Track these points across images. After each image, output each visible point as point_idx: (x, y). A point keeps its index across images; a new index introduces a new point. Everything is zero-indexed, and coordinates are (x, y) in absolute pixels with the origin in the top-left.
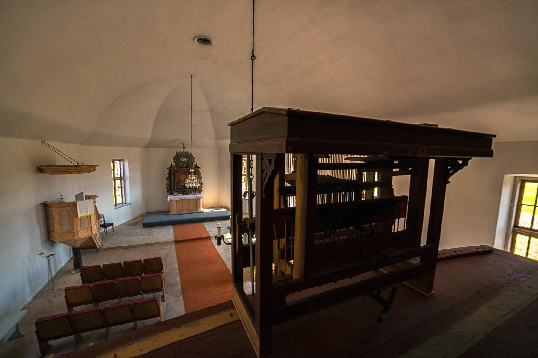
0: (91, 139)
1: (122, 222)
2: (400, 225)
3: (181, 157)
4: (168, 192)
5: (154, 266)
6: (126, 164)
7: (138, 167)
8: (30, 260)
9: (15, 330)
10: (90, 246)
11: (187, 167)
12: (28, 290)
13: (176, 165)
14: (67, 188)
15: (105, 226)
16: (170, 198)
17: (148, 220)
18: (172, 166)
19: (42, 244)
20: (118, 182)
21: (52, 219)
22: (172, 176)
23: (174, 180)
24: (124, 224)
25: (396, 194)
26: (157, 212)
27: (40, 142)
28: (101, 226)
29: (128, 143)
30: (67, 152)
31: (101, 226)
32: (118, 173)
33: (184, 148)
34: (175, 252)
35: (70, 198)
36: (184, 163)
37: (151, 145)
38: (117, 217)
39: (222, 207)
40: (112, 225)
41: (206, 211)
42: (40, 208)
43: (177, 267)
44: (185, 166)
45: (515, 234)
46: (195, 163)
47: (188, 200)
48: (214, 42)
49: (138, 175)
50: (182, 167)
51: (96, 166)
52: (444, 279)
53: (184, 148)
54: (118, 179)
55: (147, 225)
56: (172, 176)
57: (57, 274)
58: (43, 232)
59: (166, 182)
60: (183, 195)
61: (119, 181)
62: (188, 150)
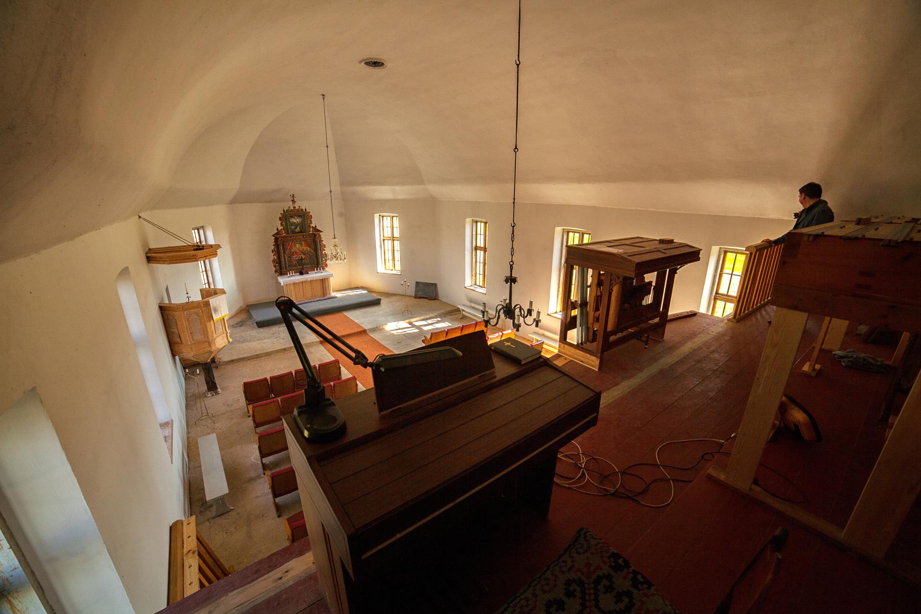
2: (649, 299)
3: (292, 217)
4: (276, 271)
11: (301, 232)
13: (286, 229)
16: (283, 280)
18: (279, 232)
22: (281, 248)
33: (293, 201)
35: (197, 297)
36: (296, 225)
39: (357, 288)
41: (339, 295)
44: (298, 230)
45: (715, 299)
46: (313, 225)
47: (312, 281)
48: (388, 64)
50: (293, 232)
52: (670, 331)
53: (293, 201)
56: (281, 248)
59: (272, 257)
60: (301, 274)
62: (301, 204)
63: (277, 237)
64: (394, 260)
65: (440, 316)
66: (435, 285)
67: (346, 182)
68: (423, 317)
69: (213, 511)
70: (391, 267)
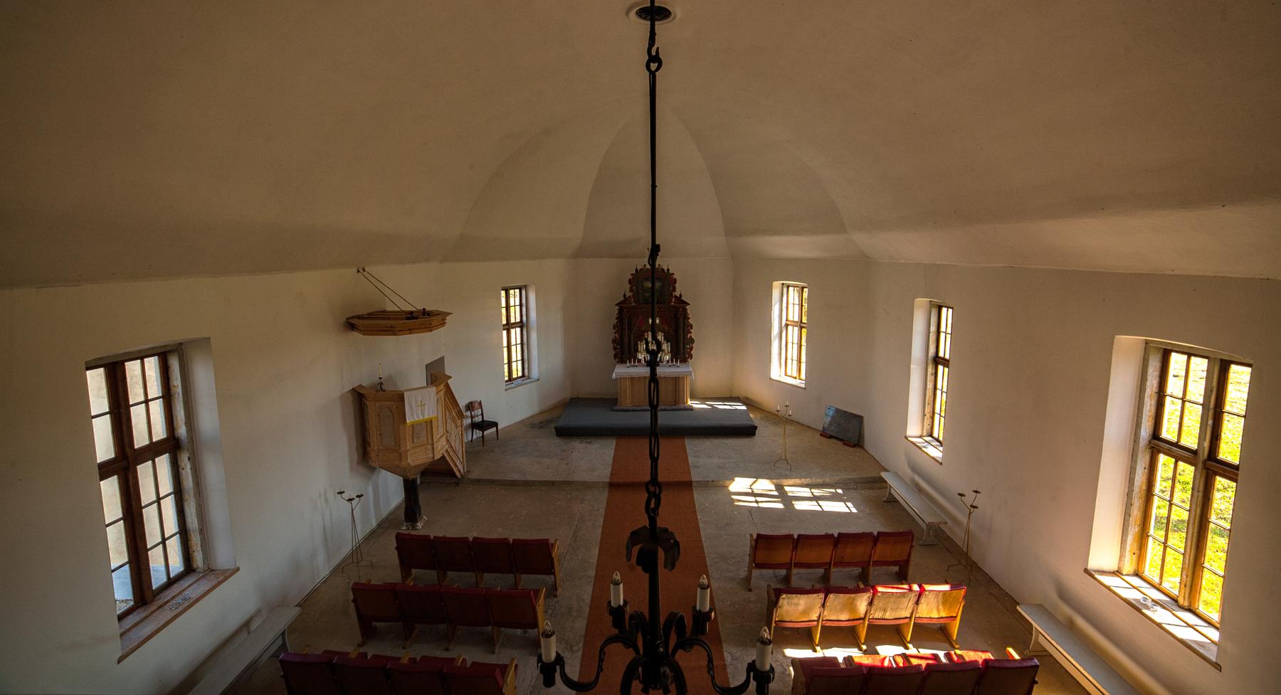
0: (461, 250)
1: (519, 419)
4: (615, 356)
5: (535, 556)
6: (532, 297)
8: (326, 500)
9: (280, 642)
10: (439, 473)
12: (321, 557)
14: (404, 358)
15: (483, 425)
17: (569, 419)
18: (626, 299)
19: (351, 469)
20: (515, 333)
21: (371, 417)
23: (630, 330)
24: (522, 422)
26: (594, 400)
27: (355, 270)
28: (474, 426)
30: (406, 286)
31: (474, 426)
32: (515, 317)
34: (602, 512)
37: (582, 253)
38: (509, 409)
39: (737, 399)
40: (495, 424)
41: (697, 405)
42: (350, 396)
43: (594, 560)
46: (677, 294)
49: (556, 318)
51: (449, 314)
54: (515, 325)
55: (565, 433)
57: (379, 526)
58: (354, 444)
59: (611, 334)
61: (518, 330)
63: (623, 306)
64: (799, 362)
65: (845, 485)
66: (860, 418)
67: (733, 230)
68: (808, 481)
69: (773, 598)
70: (795, 374)
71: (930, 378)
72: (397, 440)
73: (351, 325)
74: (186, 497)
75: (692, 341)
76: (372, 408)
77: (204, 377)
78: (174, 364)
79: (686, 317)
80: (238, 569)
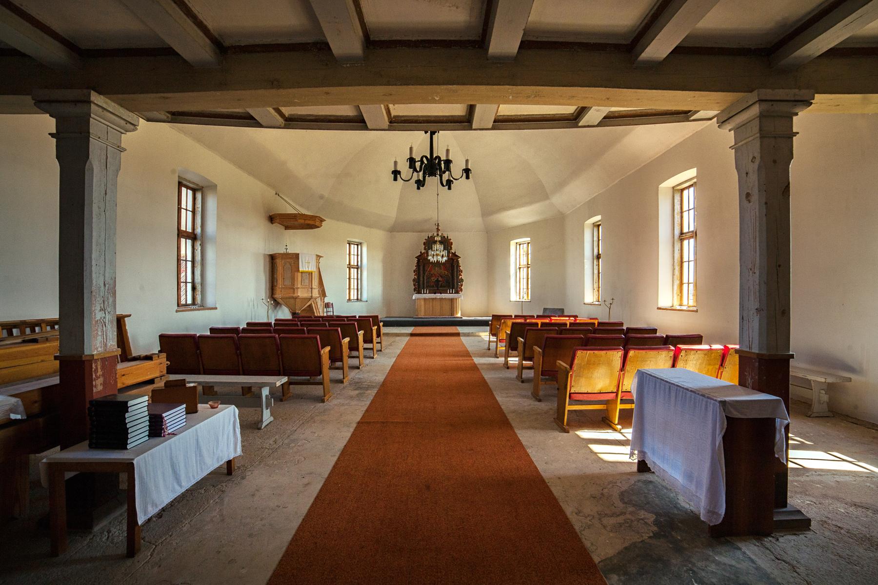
4: (415, 290)
7: (379, 255)
14: (295, 242)
21: (279, 269)
23: (424, 273)
25: (199, 406)
29: (369, 222)
37: (395, 229)
49: (379, 267)
59: (413, 276)
71: (596, 267)
72: (293, 279)
73: (272, 219)
74: (196, 265)
75: (462, 280)
76: (279, 262)
77: (212, 203)
78: (199, 196)
79: (458, 266)
80: (216, 308)
